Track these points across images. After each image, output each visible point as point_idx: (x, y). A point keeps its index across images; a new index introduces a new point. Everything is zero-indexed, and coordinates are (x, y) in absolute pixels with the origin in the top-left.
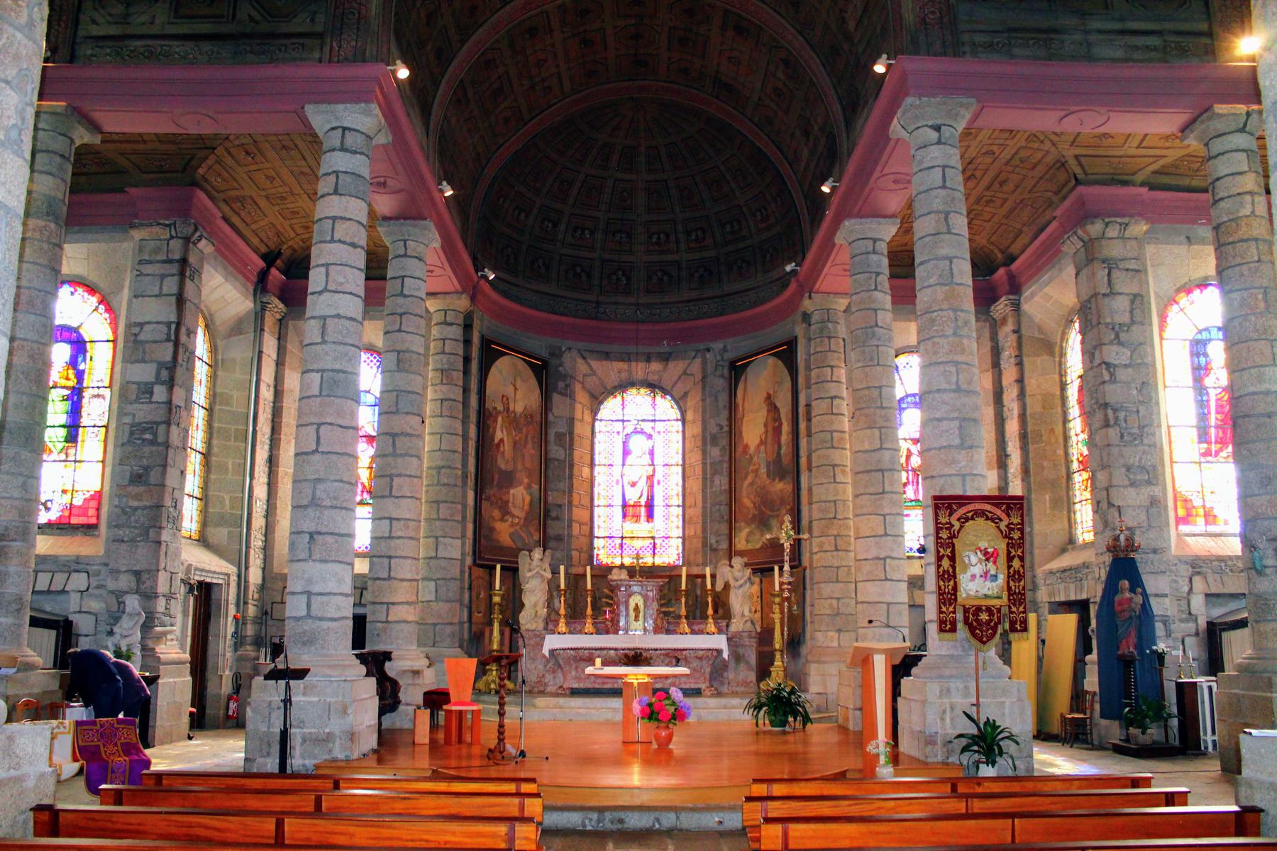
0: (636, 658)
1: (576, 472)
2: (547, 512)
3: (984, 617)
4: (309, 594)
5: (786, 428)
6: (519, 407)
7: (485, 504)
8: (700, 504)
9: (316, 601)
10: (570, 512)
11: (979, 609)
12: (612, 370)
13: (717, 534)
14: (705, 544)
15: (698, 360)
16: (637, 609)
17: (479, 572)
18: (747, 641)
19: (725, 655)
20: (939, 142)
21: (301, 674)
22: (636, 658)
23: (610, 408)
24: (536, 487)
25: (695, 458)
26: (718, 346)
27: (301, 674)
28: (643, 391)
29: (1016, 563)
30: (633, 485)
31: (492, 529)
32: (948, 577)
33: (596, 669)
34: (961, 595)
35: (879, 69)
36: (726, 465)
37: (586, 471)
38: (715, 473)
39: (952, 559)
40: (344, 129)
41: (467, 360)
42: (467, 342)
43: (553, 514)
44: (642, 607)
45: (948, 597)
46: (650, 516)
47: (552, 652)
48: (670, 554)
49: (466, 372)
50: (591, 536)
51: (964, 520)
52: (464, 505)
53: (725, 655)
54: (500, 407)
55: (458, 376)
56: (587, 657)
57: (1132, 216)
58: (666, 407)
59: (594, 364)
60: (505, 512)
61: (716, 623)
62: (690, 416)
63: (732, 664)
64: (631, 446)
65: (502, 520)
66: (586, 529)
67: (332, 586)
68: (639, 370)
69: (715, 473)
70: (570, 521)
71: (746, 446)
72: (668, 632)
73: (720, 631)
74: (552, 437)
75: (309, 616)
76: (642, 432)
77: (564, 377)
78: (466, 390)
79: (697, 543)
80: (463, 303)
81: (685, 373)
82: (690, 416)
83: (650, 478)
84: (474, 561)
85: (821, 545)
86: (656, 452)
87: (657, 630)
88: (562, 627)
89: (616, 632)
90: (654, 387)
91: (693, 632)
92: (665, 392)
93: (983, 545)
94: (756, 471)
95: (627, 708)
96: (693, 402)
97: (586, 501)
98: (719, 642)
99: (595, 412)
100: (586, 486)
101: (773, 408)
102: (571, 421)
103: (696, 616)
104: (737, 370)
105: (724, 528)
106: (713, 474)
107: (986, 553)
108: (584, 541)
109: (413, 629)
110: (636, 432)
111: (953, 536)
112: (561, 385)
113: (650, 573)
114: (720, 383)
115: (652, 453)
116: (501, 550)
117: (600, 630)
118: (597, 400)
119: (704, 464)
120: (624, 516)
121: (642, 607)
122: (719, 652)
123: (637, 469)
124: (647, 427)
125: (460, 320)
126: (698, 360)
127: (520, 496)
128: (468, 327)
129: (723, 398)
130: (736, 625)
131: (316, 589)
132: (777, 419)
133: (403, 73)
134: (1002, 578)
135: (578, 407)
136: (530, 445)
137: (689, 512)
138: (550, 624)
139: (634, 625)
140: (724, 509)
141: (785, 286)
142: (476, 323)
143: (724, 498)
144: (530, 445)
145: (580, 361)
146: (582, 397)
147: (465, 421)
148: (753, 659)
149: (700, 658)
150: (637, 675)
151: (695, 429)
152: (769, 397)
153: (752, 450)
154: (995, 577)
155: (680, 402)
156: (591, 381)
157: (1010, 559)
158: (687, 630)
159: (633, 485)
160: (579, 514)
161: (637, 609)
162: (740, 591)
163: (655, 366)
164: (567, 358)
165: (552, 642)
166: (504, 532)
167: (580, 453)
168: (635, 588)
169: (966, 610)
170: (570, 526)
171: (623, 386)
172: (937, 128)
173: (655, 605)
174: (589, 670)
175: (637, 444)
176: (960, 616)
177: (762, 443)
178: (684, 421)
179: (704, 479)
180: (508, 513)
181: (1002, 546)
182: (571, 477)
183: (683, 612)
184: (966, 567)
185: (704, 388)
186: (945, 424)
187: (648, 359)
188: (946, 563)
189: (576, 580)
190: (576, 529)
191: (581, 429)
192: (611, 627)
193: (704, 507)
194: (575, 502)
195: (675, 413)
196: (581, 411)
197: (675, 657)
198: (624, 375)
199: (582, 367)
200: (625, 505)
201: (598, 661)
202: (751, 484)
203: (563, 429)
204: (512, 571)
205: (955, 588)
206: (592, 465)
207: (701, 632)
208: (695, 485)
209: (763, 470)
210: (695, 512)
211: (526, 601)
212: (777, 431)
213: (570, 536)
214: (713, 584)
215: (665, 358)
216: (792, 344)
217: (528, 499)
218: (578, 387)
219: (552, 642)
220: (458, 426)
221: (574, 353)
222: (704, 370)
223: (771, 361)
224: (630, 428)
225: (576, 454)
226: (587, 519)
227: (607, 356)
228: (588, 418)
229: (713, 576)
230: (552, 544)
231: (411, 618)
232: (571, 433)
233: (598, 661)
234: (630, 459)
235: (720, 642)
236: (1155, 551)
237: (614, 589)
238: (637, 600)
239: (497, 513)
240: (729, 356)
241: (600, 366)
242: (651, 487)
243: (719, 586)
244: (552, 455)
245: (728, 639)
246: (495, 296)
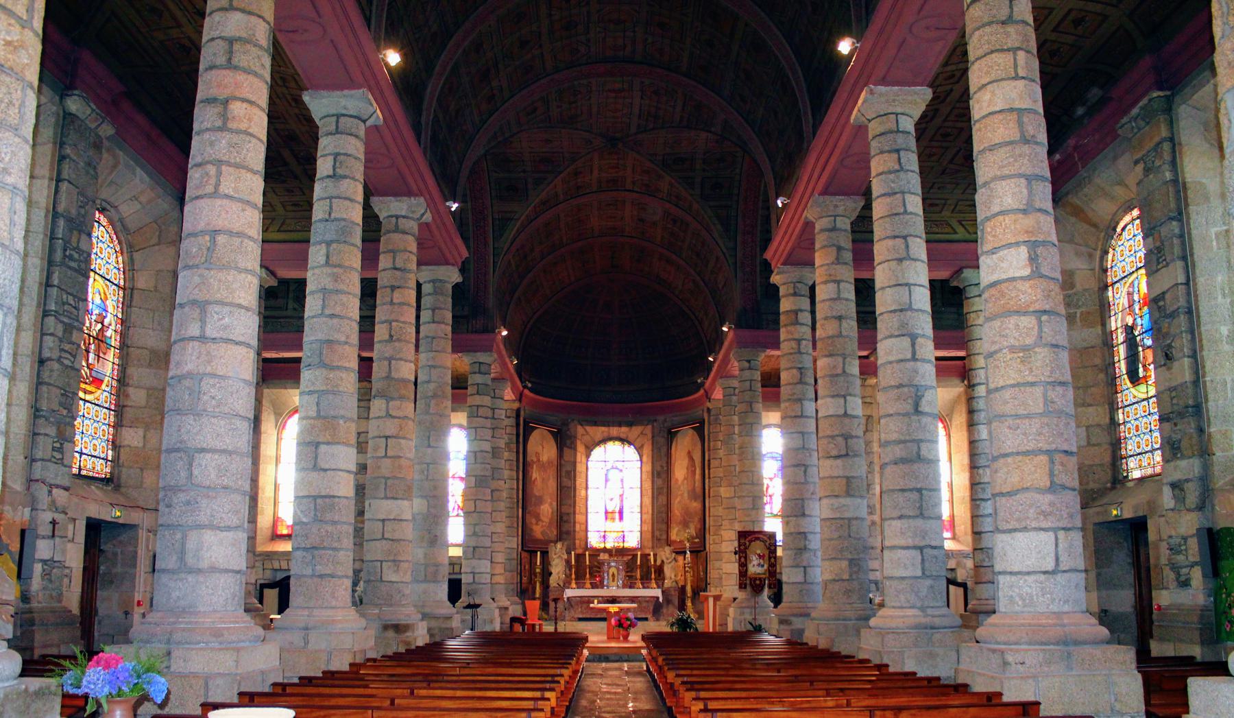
0: (613, 600)
1: (577, 493)
2: (561, 517)
3: (758, 582)
4: (474, 573)
5: (698, 471)
6: (544, 458)
7: (528, 516)
8: (650, 512)
9: (476, 576)
10: (575, 517)
11: (756, 579)
12: (600, 431)
13: (660, 530)
14: (653, 536)
15: (650, 427)
16: (613, 575)
17: (525, 555)
18: (673, 593)
19: (661, 600)
20: (750, 368)
21: (478, 606)
22: (613, 600)
23: (598, 453)
24: (555, 504)
25: (648, 485)
26: (661, 418)
27: (478, 606)
28: (617, 443)
29: (773, 560)
30: (612, 499)
31: (532, 530)
32: (743, 566)
33: (595, 605)
34: (749, 573)
35: (845, 47)
36: (665, 490)
37: (583, 492)
38: (659, 494)
39: (746, 558)
40: (480, 363)
41: (518, 435)
42: (518, 425)
43: (565, 518)
44: (616, 573)
45: (743, 573)
46: (621, 518)
47: (568, 598)
48: (632, 541)
49: (518, 442)
50: (587, 531)
51: (751, 541)
52: (518, 517)
53: (661, 600)
54: (535, 459)
55: (514, 446)
56: (589, 600)
57: (869, 374)
58: (630, 453)
59: (588, 428)
60: (538, 518)
61: (657, 583)
62: (645, 459)
63: (665, 605)
64: (610, 476)
65: (537, 524)
66: (583, 527)
67: (483, 570)
68: (614, 431)
69: (659, 494)
70: (575, 522)
71: (677, 480)
72: (630, 587)
73: (658, 587)
74: (564, 474)
75: (474, 582)
76: (616, 468)
77: (570, 437)
78: (518, 452)
79: (649, 536)
80: (516, 405)
81: (642, 433)
82: (645, 459)
83: (621, 496)
84: (522, 549)
85: (714, 540)
86: (625, 510)
87: (624, 586)
88: (574, 585)
89: (602, 588)
90: (623, 440)
91: (644, 587)
92: (630, 443)
93: (758, 552)
94: (682, 495)
95: (610, 624)
96: (647, 450)
97: (583, 510)
98: (658, 593)
99: (588, 456)
100: (584, 501)
101: (691, 459)
102: (575, 463)
103: (645, 581)
104: (671, 435)
105: (664, 527)
106: (658, 495)
107: (759, 555)
108: (583, 534)
109: (502, 587)
110: (613, 468)
111: (746, 548)
112: (568, 442)
113: (620, 552)
114: (662, 441)
115: (622, 481)
116: (537, 541)
117: (594, 586)
118: (589, 449)
119: (653, 489)
120: (606, 518)
121: (616, 573)
122: (658, 598)
123: (614, 490)
124: (619, 465)
125: (514, 415)
126: (650, 427)
127: (547, 509)
128: (518, 416)
129: (664, 450)
130: (667, 583)
131: (477, 571)
132: (694, 466)
133: (393, 58)
134: (766, 567)
135: (579, 455)
136: (551, 481)
137: (645, 516)
138: (567, 584)
139: (611, 583)
140: (664, 515)
141: (697, 390)
142: (522, 413)
143: (664, 509)
144: (551, 481)
145: (579, 427)
146: (581, 448)
147: (517, 472)
148: (676, 602)
149: (647, 602)
150: (613, 608)
151: (648, 467)
152: (689, 452)
153: (680, 482)
154: (763, 566)
155: (639, 450)
156: (587, 438)
157: (770, 558)
158: (655, 586)
159: (612, 499)
160: (579, 518)
161: (613, 575)
162: (670, 566)
163: (624, 429)
164: (572, 425)
165: (569, 593)
166: (538, 530)
167: (580, 481)
168: (613, 564)
169: (751, 579)
170: (574, 526)
171: (604, 441)
172: (749, 361)
173: (624, 573)
174: (592, 605)
175: (614, 475)
176: (748, 582)
177: (685, 479)
178: (641, 461)
179: (653, 497)
180: (540, 520)
181: (767, 552)
182: (575, 496)
183: (638, 576)
184: (751, 561)
185: (653, 444)
186: (747, 499)
187: (620, 425)
188: (743, 560)
189: (580, 557)
190: (578, 527)
191: (580, 468)
192: (600, 585)
193: (653, 515)
194: (577, 511)
195: (637, 457)
196: (580, 457)
197: (632, 599)
198: (606, 435)
199: (580, 430)
200: (606, 512)
201: (596, 601)
202: (679, 502)
203: (569, 468)
204: (545, 554)
205: (747, 570)
206: (587, 488)
207: (648, 587)
208: (648, 501)
209: (686, 495)
210: (648, 517)
211: (553, 571)
212: (694, 472)
213: (574, 531)
214: (655, 561)
215: (630, 425)
216: (702, 423)
217: (550, 511)
218: (578, 442)
219: (569, 593)
220: (514, 474)
221: (576, 422)
222: (653, 433)
223: (691, 432)
224: (609, 465)
225: (578, 483)
226: (584, 521)
227: (595, 424)
228: (584, 460)
229: (655, 555)
230: (565, 536)
231: (502, 582)
232: (575, 470)
233: (596, 601)
234: (609, 483)
235: (658, 593)
236: (872, 548)
237: (601, 564)
238: (613, 570)
239: (534, 521)
240: (667, 424)
241: (591, 430)
242: (622, 501)
243: (659, 563)
244: (564, 484)
245: (663, 592)
246: (532, 395)
